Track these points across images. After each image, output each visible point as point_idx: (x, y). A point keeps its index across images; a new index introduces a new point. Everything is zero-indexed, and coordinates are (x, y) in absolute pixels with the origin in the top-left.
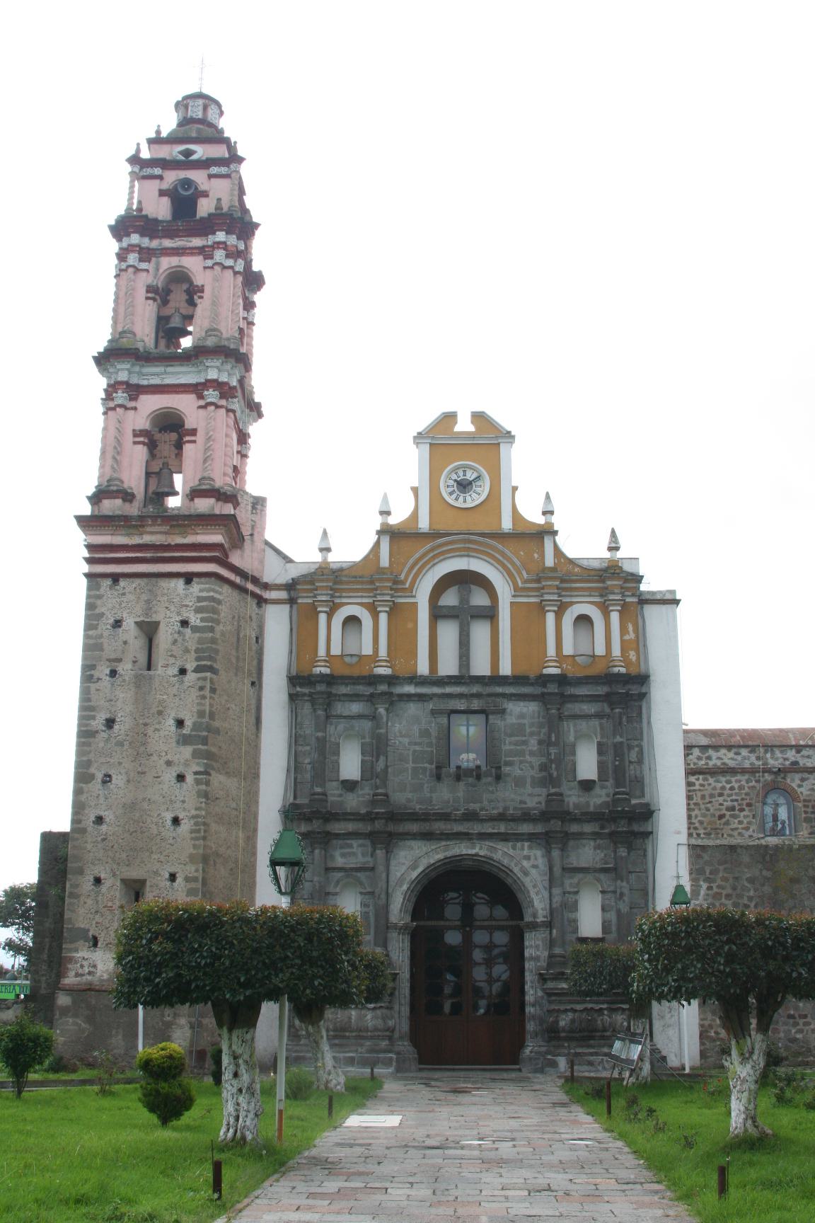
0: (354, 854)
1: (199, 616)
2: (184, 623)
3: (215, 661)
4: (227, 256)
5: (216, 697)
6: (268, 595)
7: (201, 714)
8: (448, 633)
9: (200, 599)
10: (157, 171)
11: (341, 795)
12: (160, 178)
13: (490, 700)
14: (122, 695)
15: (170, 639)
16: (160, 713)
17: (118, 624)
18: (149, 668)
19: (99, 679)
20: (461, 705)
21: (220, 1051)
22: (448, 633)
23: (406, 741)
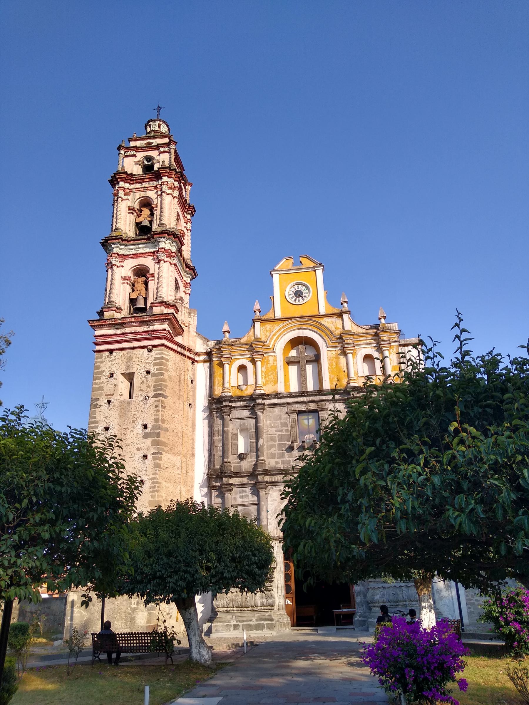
0: (247, 496)
1: (156, 367)
2: (148, 372)
3: (165, 391)
4: (169, 189)
5: (165, 411)
6: (197, 358)
7: (157, 420)
8: (293, 370)
9: (156, 359)
10: (133, 153)
11: (239, 463)
12: (135, 156)
15: (140, 381)
16: (134, 422)
17: (112, 375)
18: (130, 398)
19: (100, 406)
20: (303, 407)
21: (127, 652)
22: (293, 370)
23: (275, 429)
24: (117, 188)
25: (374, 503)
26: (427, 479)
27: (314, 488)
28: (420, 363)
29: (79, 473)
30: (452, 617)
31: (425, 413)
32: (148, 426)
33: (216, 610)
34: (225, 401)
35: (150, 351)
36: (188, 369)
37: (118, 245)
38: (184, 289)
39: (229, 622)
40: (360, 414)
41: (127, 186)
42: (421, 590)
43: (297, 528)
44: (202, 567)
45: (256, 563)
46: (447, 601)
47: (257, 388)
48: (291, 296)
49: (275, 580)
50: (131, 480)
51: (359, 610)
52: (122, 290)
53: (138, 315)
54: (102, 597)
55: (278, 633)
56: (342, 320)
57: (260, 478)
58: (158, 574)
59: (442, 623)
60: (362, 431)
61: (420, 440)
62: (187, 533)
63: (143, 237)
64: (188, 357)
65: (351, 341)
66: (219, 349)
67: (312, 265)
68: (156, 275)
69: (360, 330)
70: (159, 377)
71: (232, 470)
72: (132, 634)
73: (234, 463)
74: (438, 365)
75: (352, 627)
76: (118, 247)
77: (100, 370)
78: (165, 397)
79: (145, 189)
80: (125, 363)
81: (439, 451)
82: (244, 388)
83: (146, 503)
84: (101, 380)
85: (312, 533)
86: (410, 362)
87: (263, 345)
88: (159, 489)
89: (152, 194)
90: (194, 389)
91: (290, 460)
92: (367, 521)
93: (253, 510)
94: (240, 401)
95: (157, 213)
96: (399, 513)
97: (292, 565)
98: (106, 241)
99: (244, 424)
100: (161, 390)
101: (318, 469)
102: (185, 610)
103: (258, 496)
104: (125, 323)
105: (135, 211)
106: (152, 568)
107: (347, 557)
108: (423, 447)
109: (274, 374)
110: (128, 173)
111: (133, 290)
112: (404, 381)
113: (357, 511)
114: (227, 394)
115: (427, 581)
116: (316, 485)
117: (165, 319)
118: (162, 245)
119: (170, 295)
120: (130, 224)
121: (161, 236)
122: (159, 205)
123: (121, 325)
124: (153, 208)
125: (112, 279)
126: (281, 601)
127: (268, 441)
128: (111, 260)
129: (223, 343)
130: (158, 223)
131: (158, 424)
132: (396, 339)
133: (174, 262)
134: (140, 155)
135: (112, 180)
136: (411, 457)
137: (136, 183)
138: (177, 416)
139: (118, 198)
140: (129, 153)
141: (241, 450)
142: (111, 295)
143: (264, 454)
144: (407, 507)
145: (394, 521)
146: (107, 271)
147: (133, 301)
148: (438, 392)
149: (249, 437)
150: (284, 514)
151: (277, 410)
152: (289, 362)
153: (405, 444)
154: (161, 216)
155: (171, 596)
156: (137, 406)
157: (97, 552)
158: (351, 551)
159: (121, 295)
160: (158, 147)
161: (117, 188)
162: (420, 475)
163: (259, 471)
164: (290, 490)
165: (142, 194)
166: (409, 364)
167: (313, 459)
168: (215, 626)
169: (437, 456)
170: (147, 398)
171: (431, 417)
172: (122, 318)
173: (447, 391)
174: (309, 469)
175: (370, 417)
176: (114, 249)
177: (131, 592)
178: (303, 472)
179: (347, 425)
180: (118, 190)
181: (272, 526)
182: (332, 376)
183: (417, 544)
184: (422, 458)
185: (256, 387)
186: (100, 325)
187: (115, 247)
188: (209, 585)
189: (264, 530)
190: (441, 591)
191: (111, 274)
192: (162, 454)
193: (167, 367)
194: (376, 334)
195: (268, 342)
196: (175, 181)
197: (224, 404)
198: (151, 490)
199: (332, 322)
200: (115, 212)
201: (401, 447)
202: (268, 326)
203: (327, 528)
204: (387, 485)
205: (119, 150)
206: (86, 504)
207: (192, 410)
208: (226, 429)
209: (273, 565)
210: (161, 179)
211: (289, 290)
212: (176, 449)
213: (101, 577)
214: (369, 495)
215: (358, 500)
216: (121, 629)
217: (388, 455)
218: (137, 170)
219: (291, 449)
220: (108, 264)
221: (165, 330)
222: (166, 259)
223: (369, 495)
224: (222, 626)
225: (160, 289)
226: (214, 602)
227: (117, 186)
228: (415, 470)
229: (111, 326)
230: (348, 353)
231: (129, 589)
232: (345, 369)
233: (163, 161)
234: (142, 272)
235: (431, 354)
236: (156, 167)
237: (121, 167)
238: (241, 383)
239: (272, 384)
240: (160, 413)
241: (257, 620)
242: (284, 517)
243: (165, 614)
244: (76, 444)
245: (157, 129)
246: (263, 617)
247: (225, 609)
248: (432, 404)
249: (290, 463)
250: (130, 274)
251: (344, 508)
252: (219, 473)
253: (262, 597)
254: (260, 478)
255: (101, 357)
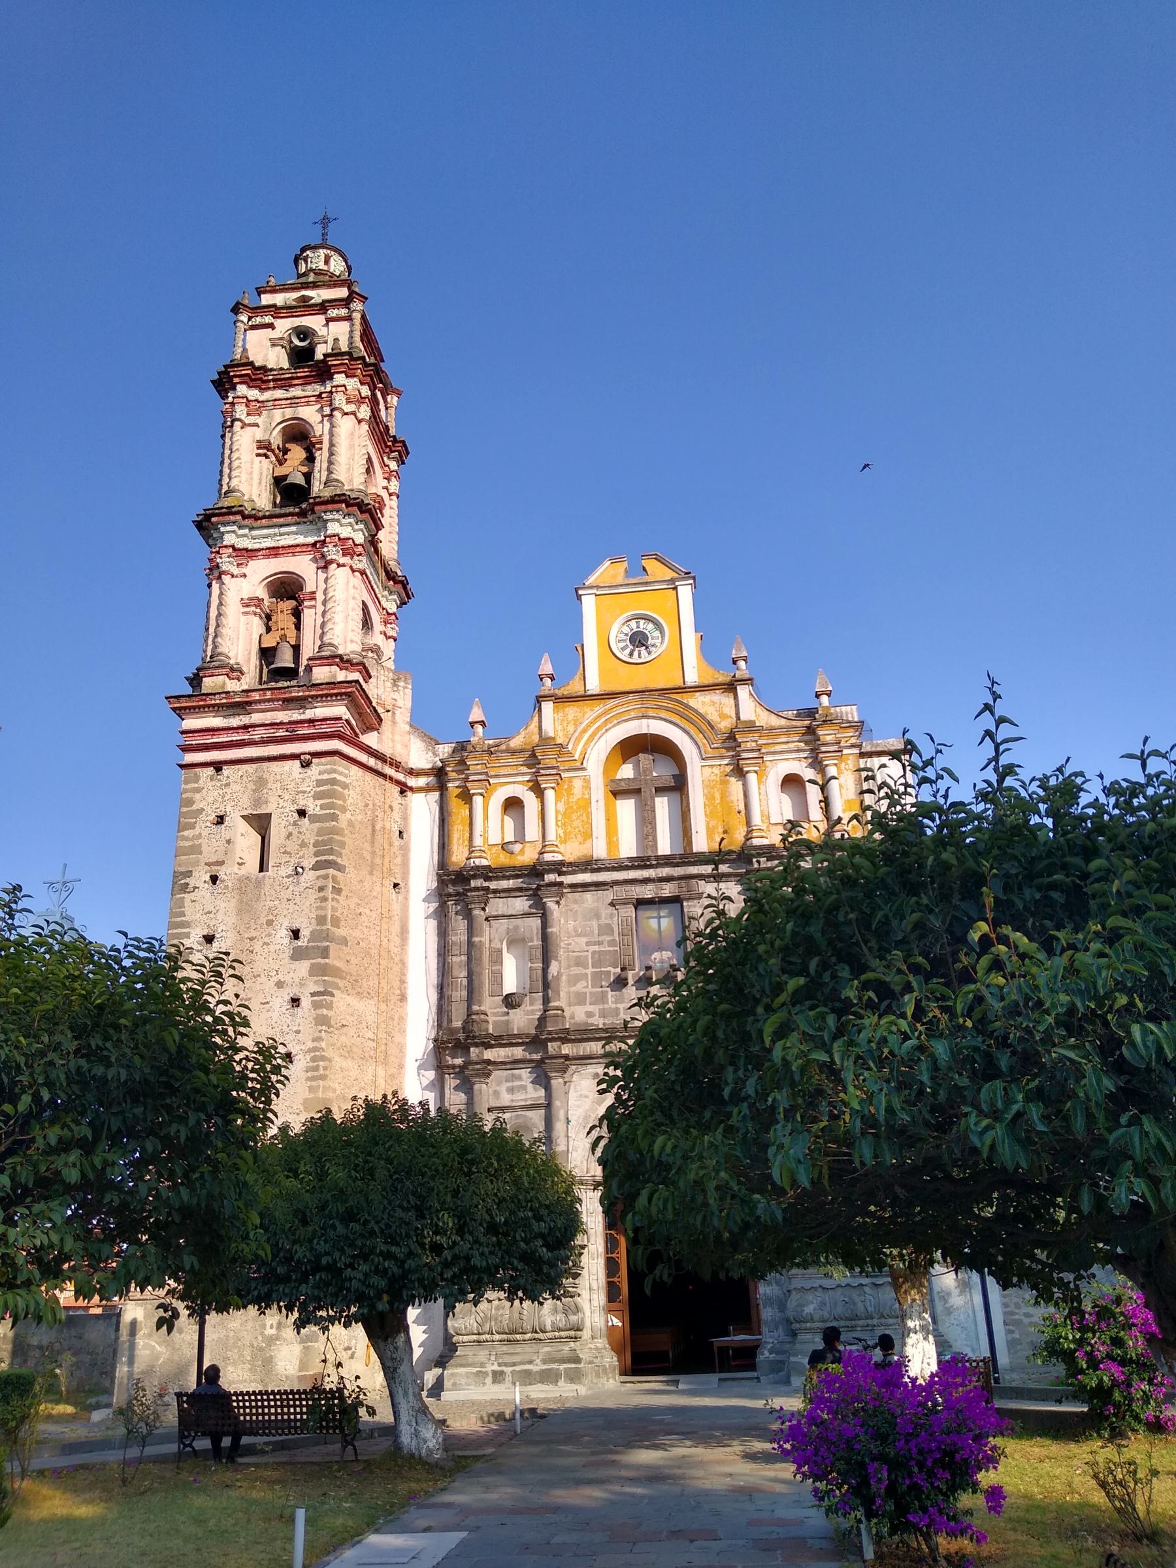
0: (524, 1088)
2: (302, 813)
3: (340, 855)
4: (348, 402)
6: (412, 782)
7: (321, 920)
8: (626, 809)
9: (320, 783)
10: (268, 319)
12: (271, 326)
13: (683, 883)
14: (223, 905)
15: (284, 833)
17: (220, 820)
18: (261, 870)
19: (195, 888)
20: (648, 892)
22: (626, 809)
23: (585, 940)
24: (230, 399)
25: (805, 1101)
26: (921, 1048)
27: (672, 1069)
28: (905, 793)
29: (146, 1037)
30: (973, 1350)
31: (917, 903)
32: (302, 933)
33: (454, 1340)
34: (475, 877)
35: (306, 765)
36: (391, 807)
37: (235, 528)
38: (382, 628)
39: (482, 1365)
40: (776, 904)
41: (253, 394)
42: (905, 1292)
43: (633, 1156)
44: (422, 1245)
45: (541, 1235)
46: (962, 1317)
47: (547, 849)
48: (622, 645)
49: (585, 1273)
50: (265, 1051)
51: (770, 1339)
52: (242, 628)
53: (280, 685)
54: (199, 1314)
55: (590, 1388)
56: (736, 697)
57: (552, 1047)
58: (324, 1261)
59: (951, 1367)
60: (778, 943)
61: (905, 962)
62: (389, 1171)
63: (291, 509)
64: (391, 778)
65: (754, 744)
66: (462, 762)
67: (670, 574)
68: (320, 597)
69: (775, 721)
70: (328, 824)
71: (491, 1031)
72: (267, 1393)
73: (495, 1014)
74: (946, 797)
75: (755, 1374)
76: (234, 532)
77: (195, 807)
78: (340, 868)
79: (294, 402)
80: (249, 792)
81: (946, 985)
82: (517, 847)
83: (298, 1105)
84: (197, 831)
85: (668, 1167)
86: (886, 790)
87: (560, 754)
88: (327, 1072)
89: (310, 413)
90: (405, 850)
91: (618, 1009)
92: (786, 1141)
93: (536, 1118)
94: (508, 878)
95: (321, 457)
96: (858, 1123)
97: (623, 1241)
98: (208, 517)
99: (516, 928)
100: (331, 852)
101: (680, 1027)
102: (386, 1340)
103: (548, 1088)
104: (250, 703)
105: (273, 451)
106: (312, 1249)
107: (742, 1220)
108: (911, 978)
109: (584, 818)
110: (257, 364)
111: (268, 630)
112: (871, 833)
113: (766, 1118)
114: (478, 862)
115: (918, 1272)
116: (676, 1063)
117: (341, 694)
118: (333, 528)
119: (352, 641)
120: (260, 479)
121: (330, 507)
122: (326, 439)
123: (241, 706)
124: (313, 445)
125: (221, 604)
126: (597, 1319)
127: (569, 967)
128: (219, 560)
129: (469, 748)
130: (324, 479)
131: (324, 927)
132: (853, 740)
133: (360, 566)
134: (283, 326)
135: (220, 379)
136: (885, 998)
137: (274, 388)
138: (368, 911)
139: (233, 421)
140: (258, 320)
141: (510, 985)
142: (219, 639)
143: (562, 994)
144: (877, 1109)
145: (848, 1140)
146: (210, 586)
147: (267, 654)
148: (945, 856)
149: (527, 958)
150: (605, 1127)
151: (589, 897)
152: (618, 792)
153: (874, 971)
154: (330, 463)
155: (353, 1309)
156: (277, 888)
157: (186, 1212)
158: (752, 1206)
159: (240, 638)
160: (323, 307)
161: (230, 399)
162: (906, 1037)
163: (550, 1033)
164: (619, 1073)
165: (289, 413)
166: (882, 793)
167: (670, 1005)
168: (452, 1374)
169: (944, 998)
170: (300, 870)
171: (931, 911)
172: (243, 691)
173: (966, 853)
174: (660, 1027)
175: (796, 911)
176: (226, 537)
177: (263, 1301)
178: (648, 1035)
179: (746, 928)
180: (233, 404)
181: (579, 1155)
182: (712, 823)
183: (898, 1189)
184: (910, 1001)
185: (544, 847)
186: (194, 708)
187: (228, 532)
188: (438, 1285)
189: (560, 1161)
190: (949, 1294)
191: (218, 592)
192: (333, 995)
193: (345, 801)
194: (810, 730)
195: (570, 747)
196: (362, 384)
197: (473, 883)
198: (309, 1074)
199: (713, 703)
200: (227, 452)
201: (863, 977)
202: (571, 710)
203: (701, 1158)
204: (833, 1062)
205: (236, 314)
206: (162, 1106)
207: (400, 897)
208: (476, 939)
209: (580, 1240)
210: (331, 379)
211: (618, 632)
212: (365, 984)
213: (197, 1266)
214: (793, 1084)
215: (768, 1095)
216: (241, 1382)
217: (835, 995)
218: (277, 359)
219: (620, 983)
220: (210, 569)
221: (340, 719)
222: (342, 560)
223: (793, 1084)
224: (468, 1375)
225: (328, 626)
226: (449, 1323)
227: (231, 395)
228: (894, 1028)
229: (217, 709)
230: (748, 772)
231: (259, 1294)
232: (742, 807)
233: (336, 340)
234: (287, 589)
235: (930, 773)
236: (320, 352)
237: (240, 350)
238: (510, 836)
239: (580, 838)
240: (330, 904)
241: (544, 1362)
242: (604, 1131)
243: (339, 1348)
244: (139, 972)
245: (322, 266)
246: (559, 1355)
247: (475, 1337)
248: (932, 883)
249: (618, 1015)
250: (262, 592)
251: (738, 1114)
252: (461, 1036)
253: (555, 1311)
254: (552, 1047)
255: (197, 779)
